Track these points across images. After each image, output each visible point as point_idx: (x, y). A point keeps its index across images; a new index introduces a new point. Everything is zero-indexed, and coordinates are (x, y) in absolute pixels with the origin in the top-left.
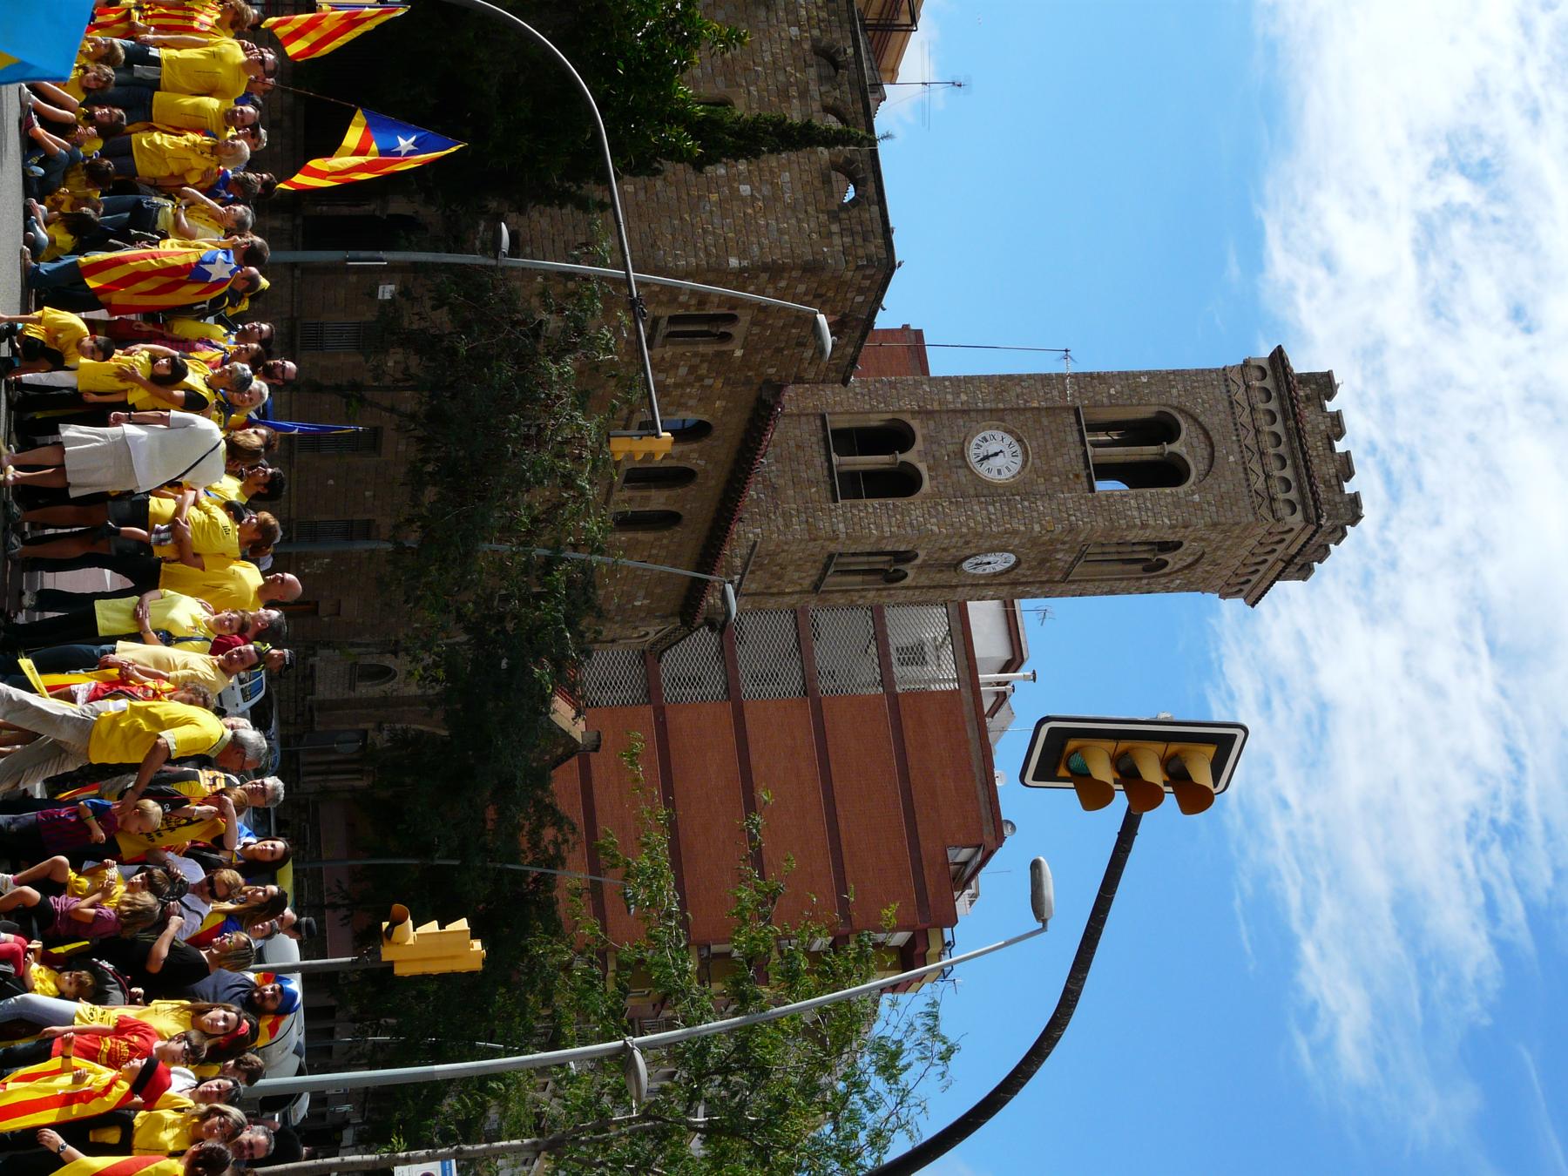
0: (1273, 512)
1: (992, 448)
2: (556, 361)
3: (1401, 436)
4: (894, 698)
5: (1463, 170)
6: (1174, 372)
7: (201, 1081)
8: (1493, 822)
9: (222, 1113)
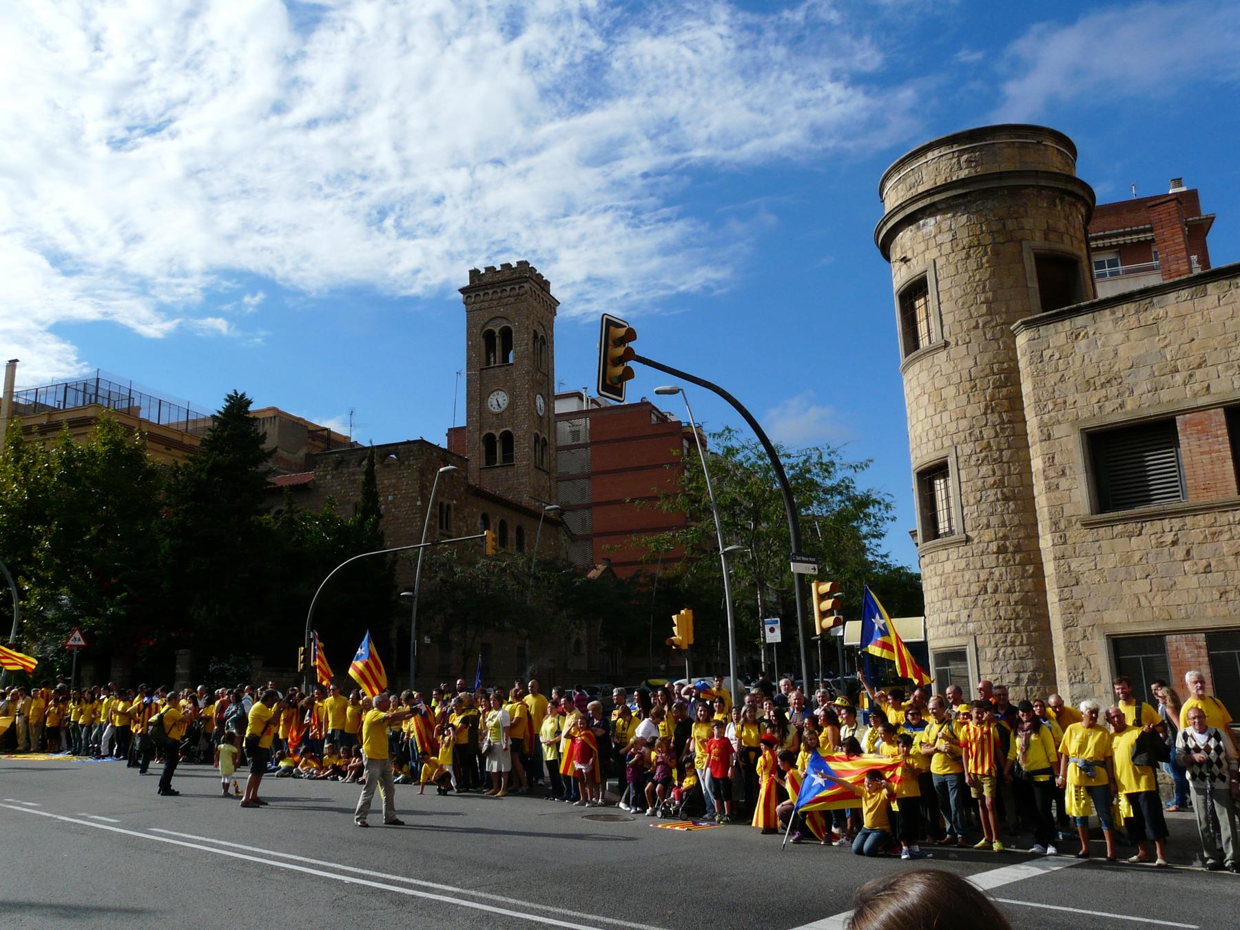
0: (523, 295)
1: (495, 403)
2: (456, 574)
3: (484, 247)
4: (592, 443)
5: (381, 221)
6: (467, 331)
7: (732, 721)
8: (632, 218)
9: (745, 712)
